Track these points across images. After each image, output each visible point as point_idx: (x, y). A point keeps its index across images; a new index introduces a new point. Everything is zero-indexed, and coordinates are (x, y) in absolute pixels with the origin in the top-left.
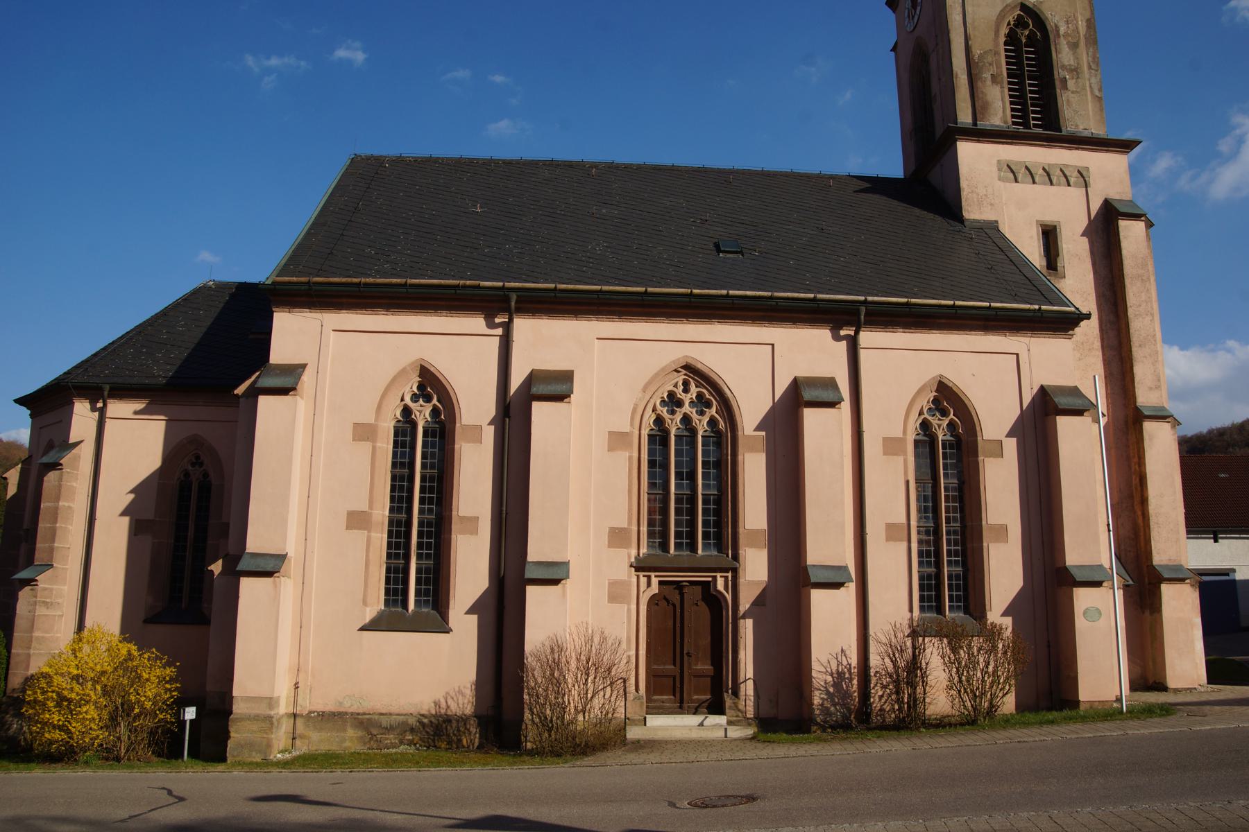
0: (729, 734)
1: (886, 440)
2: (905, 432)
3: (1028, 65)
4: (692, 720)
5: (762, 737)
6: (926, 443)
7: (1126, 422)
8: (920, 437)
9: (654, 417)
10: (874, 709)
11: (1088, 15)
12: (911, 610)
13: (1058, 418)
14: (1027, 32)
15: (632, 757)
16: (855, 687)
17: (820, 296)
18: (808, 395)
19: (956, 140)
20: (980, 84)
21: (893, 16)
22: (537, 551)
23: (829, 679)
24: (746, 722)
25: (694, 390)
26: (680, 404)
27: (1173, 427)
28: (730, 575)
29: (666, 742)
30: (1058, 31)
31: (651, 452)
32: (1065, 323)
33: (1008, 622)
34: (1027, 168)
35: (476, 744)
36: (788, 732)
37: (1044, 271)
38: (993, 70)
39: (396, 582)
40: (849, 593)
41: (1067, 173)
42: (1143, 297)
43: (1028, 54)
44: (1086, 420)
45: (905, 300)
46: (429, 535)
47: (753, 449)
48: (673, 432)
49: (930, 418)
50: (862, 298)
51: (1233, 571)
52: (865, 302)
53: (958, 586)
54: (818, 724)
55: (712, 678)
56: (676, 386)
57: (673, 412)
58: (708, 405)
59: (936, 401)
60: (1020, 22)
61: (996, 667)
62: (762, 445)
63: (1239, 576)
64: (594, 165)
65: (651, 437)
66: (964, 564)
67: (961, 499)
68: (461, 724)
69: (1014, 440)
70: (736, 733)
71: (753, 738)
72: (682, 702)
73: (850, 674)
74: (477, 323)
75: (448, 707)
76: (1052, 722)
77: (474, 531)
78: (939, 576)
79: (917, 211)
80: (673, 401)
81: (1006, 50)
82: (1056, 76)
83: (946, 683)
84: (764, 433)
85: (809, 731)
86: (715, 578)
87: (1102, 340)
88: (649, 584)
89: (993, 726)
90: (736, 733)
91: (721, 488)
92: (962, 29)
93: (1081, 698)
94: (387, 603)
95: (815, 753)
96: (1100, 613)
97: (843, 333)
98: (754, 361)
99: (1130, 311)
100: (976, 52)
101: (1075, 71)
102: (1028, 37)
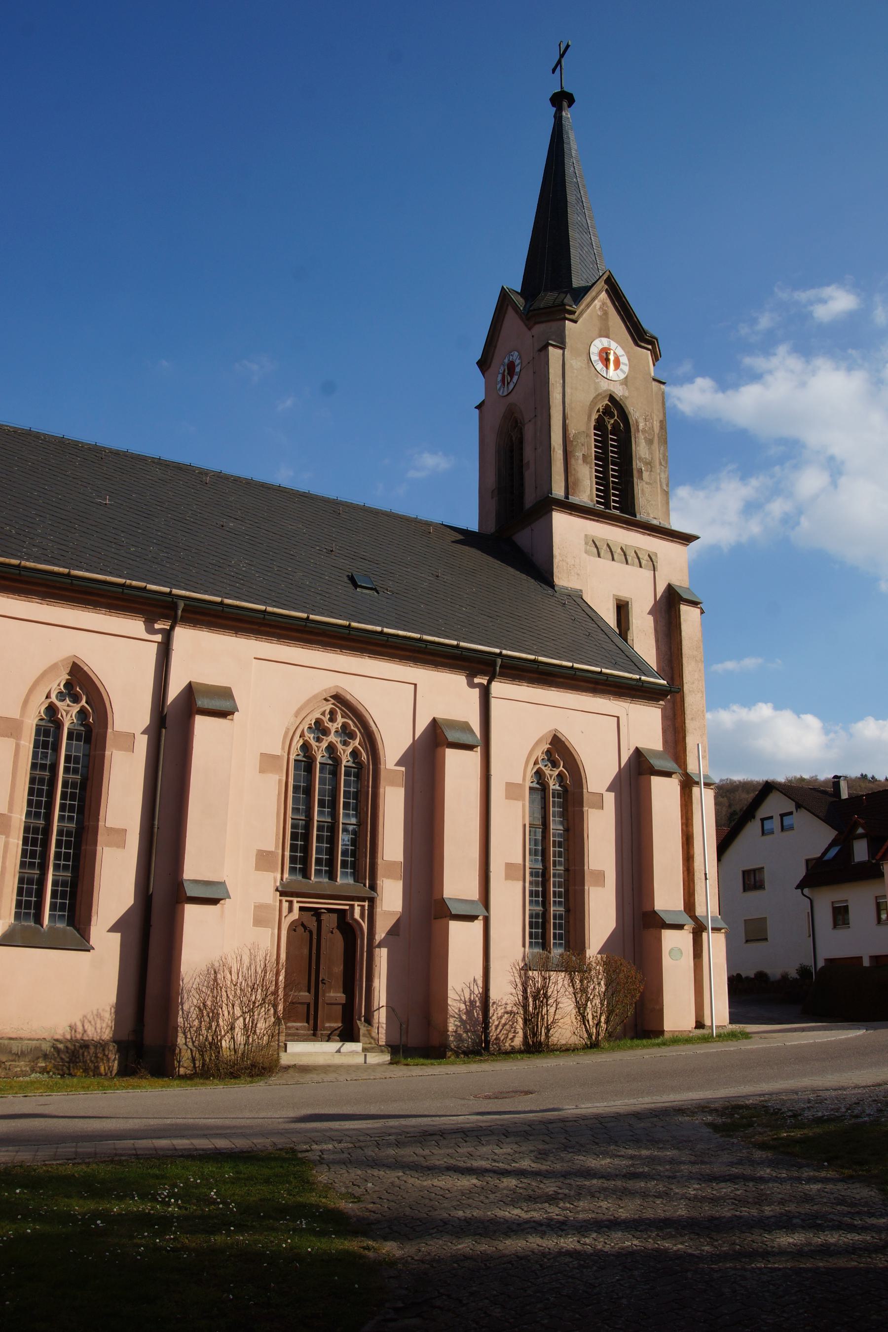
0: (369, 1060)
2: (524, 779)
11: (661, 417)
12: (524, 946)
14: (612, 421)
19: (552, 510)
20: (573, 461)
22: (194, 868)
23: (463, 1007)
24: (380, 1049)
25: (340, 720)
26: (326, 732)
28: (366, 904)
30: (638, 426)
34: (608, 545)
35: (115, 1072)
38: (584, 451)
39: (29, 894)
46: (68, 845)
47: (393, 784)
48: (319, 759)
50: (497, 651)
52: (500, 654)
54: (452, 1050)
58: (352, 736)
59: (548, 752)
60: (607, 411)
62: (401, 779)
64: (203, 473)
68: (99, 1050)
69: (613, 794)
70: (374, 1059)
72: (315, 1029)
74: (135, 626)
75: (85, 1031)
77: (122, 844)
80: (319, 728)
82: (634, 466)
84: (403, 769)
86: (352, 906)
88: (290, 910)
93: (667, 1027)
94: (17, 916)
96: (682, 953)
97: (476, 680)
98: (402, 700)
100: (572, 431)
101: (649, 464)
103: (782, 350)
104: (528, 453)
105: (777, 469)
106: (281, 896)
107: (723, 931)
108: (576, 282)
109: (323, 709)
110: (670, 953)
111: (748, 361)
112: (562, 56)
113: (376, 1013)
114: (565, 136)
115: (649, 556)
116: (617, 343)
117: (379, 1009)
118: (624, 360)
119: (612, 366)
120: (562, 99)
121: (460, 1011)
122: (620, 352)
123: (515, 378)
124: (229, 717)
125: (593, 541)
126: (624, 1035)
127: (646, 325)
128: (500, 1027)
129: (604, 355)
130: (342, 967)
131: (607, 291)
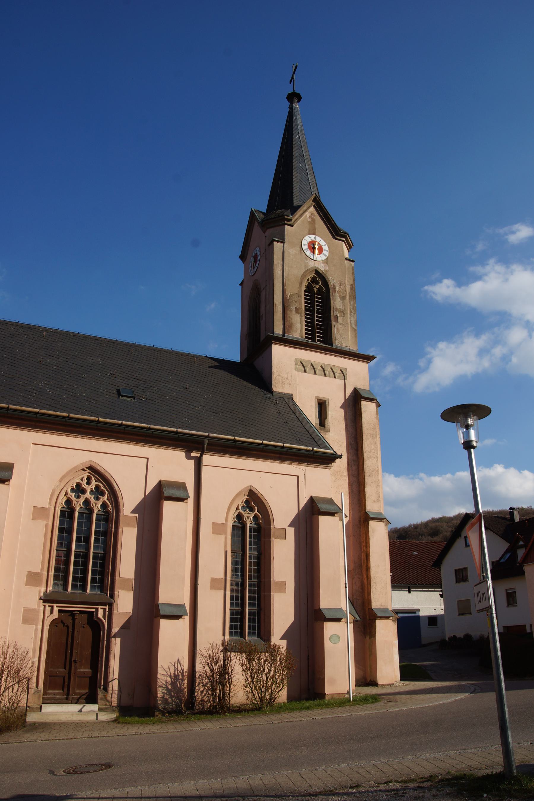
0: (99, 718)
1: (215, 524)
3: (317, 305)
4: (74, 708)
5: (122, 719)
6: (239, 527)
7: (360, 521)
8: (236, 524)
9: (65, 499)
10: (198, 700)
11: (351, 282)
12: (224, 635)
13: (319, 516)
14: (318, 287)
15: (29, 736)
16: (186, 685)
17: (180, 430)
18: (167, 492)
19: (272, 343)
20: (289, 312)
21: (243, 265)
23: (169, 679)
24: (111, 709)
26: (84, 491)
27: (386, 525)
28: (107, 607)
29: (55, 724)
30: (335, 289)
31: (61, 522)
32: (327, 459)
33: (283, 644)
34: (312, 364)
36: (139, 716)
37: (318, 427)
38: (297, 305)
40: (185, 622)
41: (335, 371)
42: (373, 447)
43: (317, 299)
44: (336, 518)
45: (232, 438)
47: (129, 525)
48: (77, 510)
49: (243, 512)
50: (206, 434)
51: (419, 610)
52: (208, 437)
53: (254, 619)
54: (159, 710)
55: (91, 678)
56: (82, 480)
57: (78, 497)
58: (103, 494)
60: (314, 280)
61: (275, 672)
62: (135, 522)
63: (421, 614)
64: (45, 329)
65: (62, 513)
66: (259, 605)
67: (259, 564)
70: (104, 717)
71: (116, 720)
72: (68, 694)
73: (183, 676)
76: (308, 708)
78: (242, 613)
79: (245, 383)
80: (79, 490)
81: (305, 295)
82: (332, 314)
83: (243, 683)
84: (137, 515)
85: (153, 716)
86: (97, 609)
87: (349, 470)
88: (52, 612)
89: (271, 712)
90: (104, 717)
91: (106, 549)
92: (281, 279)
93: (327, 692)
95: (156, 731)
98: (135, 468)
99: (365, 455)
100: (288, 293)
101: (343, 312)
102: (318, 289)
103: (492, 261)
104: (263, 310)
105: (496, 329)
106: (43, 602)
107: (391, 618)
108: (296, 203)
109: (82, 476)
110: (330, 638)
111: (472, 269)
112: (294, 73)
113: (111, 684)
114: (294, 118)
115: (341, 370)
116: (321, 237)
117: (113, 680)
118: (325, 248)
119: (317, 251)
120: (294, 97)
121: (166, 682)
122: (323, 243)
123: (258, 263)
124: (6, 483)
125: (301, 362)
126: (299, 699)
127: (341, 224)
128: (205, 692)
129: (312, 245)
130: (90, 651)
131: (314, 206)
